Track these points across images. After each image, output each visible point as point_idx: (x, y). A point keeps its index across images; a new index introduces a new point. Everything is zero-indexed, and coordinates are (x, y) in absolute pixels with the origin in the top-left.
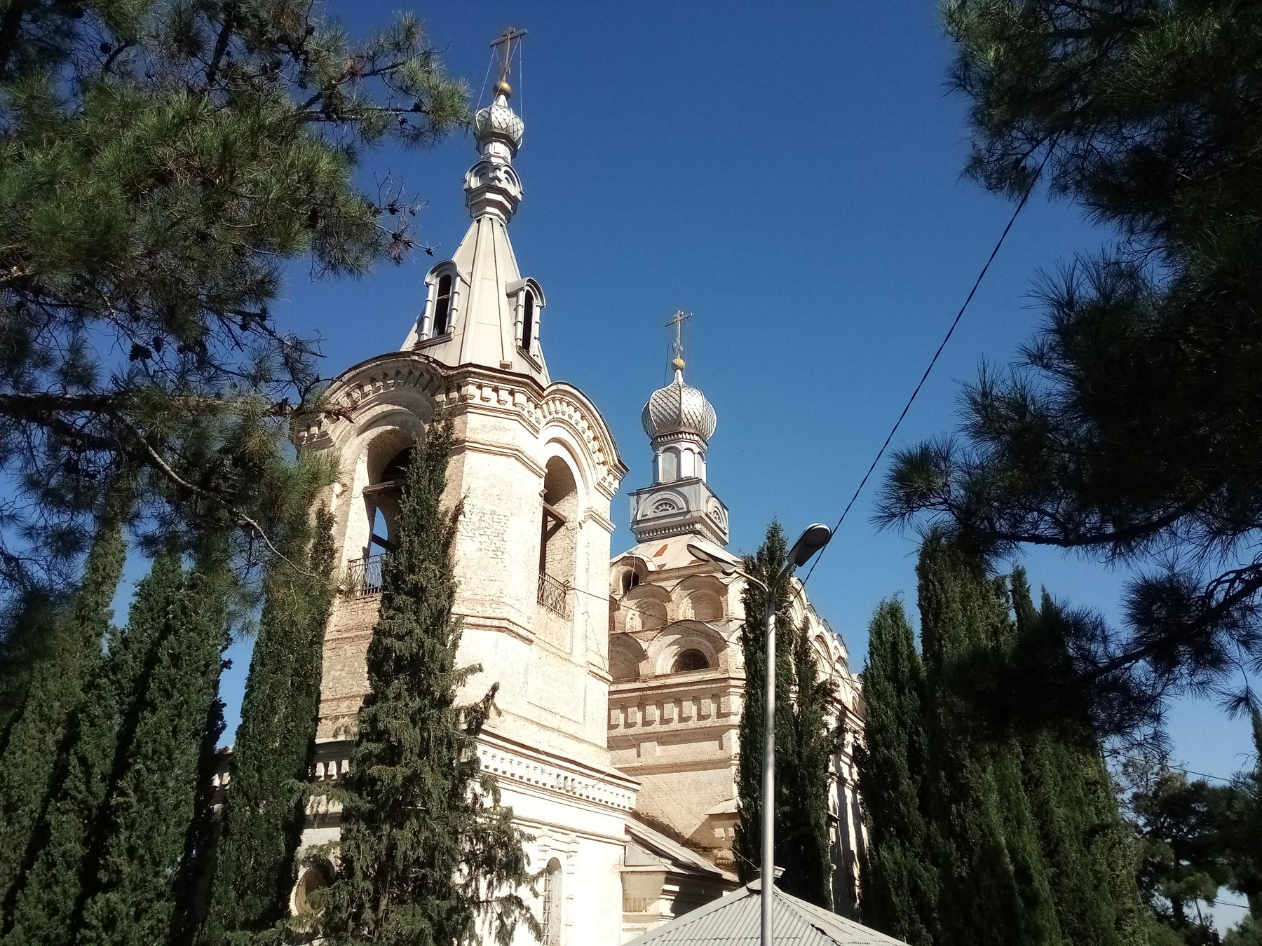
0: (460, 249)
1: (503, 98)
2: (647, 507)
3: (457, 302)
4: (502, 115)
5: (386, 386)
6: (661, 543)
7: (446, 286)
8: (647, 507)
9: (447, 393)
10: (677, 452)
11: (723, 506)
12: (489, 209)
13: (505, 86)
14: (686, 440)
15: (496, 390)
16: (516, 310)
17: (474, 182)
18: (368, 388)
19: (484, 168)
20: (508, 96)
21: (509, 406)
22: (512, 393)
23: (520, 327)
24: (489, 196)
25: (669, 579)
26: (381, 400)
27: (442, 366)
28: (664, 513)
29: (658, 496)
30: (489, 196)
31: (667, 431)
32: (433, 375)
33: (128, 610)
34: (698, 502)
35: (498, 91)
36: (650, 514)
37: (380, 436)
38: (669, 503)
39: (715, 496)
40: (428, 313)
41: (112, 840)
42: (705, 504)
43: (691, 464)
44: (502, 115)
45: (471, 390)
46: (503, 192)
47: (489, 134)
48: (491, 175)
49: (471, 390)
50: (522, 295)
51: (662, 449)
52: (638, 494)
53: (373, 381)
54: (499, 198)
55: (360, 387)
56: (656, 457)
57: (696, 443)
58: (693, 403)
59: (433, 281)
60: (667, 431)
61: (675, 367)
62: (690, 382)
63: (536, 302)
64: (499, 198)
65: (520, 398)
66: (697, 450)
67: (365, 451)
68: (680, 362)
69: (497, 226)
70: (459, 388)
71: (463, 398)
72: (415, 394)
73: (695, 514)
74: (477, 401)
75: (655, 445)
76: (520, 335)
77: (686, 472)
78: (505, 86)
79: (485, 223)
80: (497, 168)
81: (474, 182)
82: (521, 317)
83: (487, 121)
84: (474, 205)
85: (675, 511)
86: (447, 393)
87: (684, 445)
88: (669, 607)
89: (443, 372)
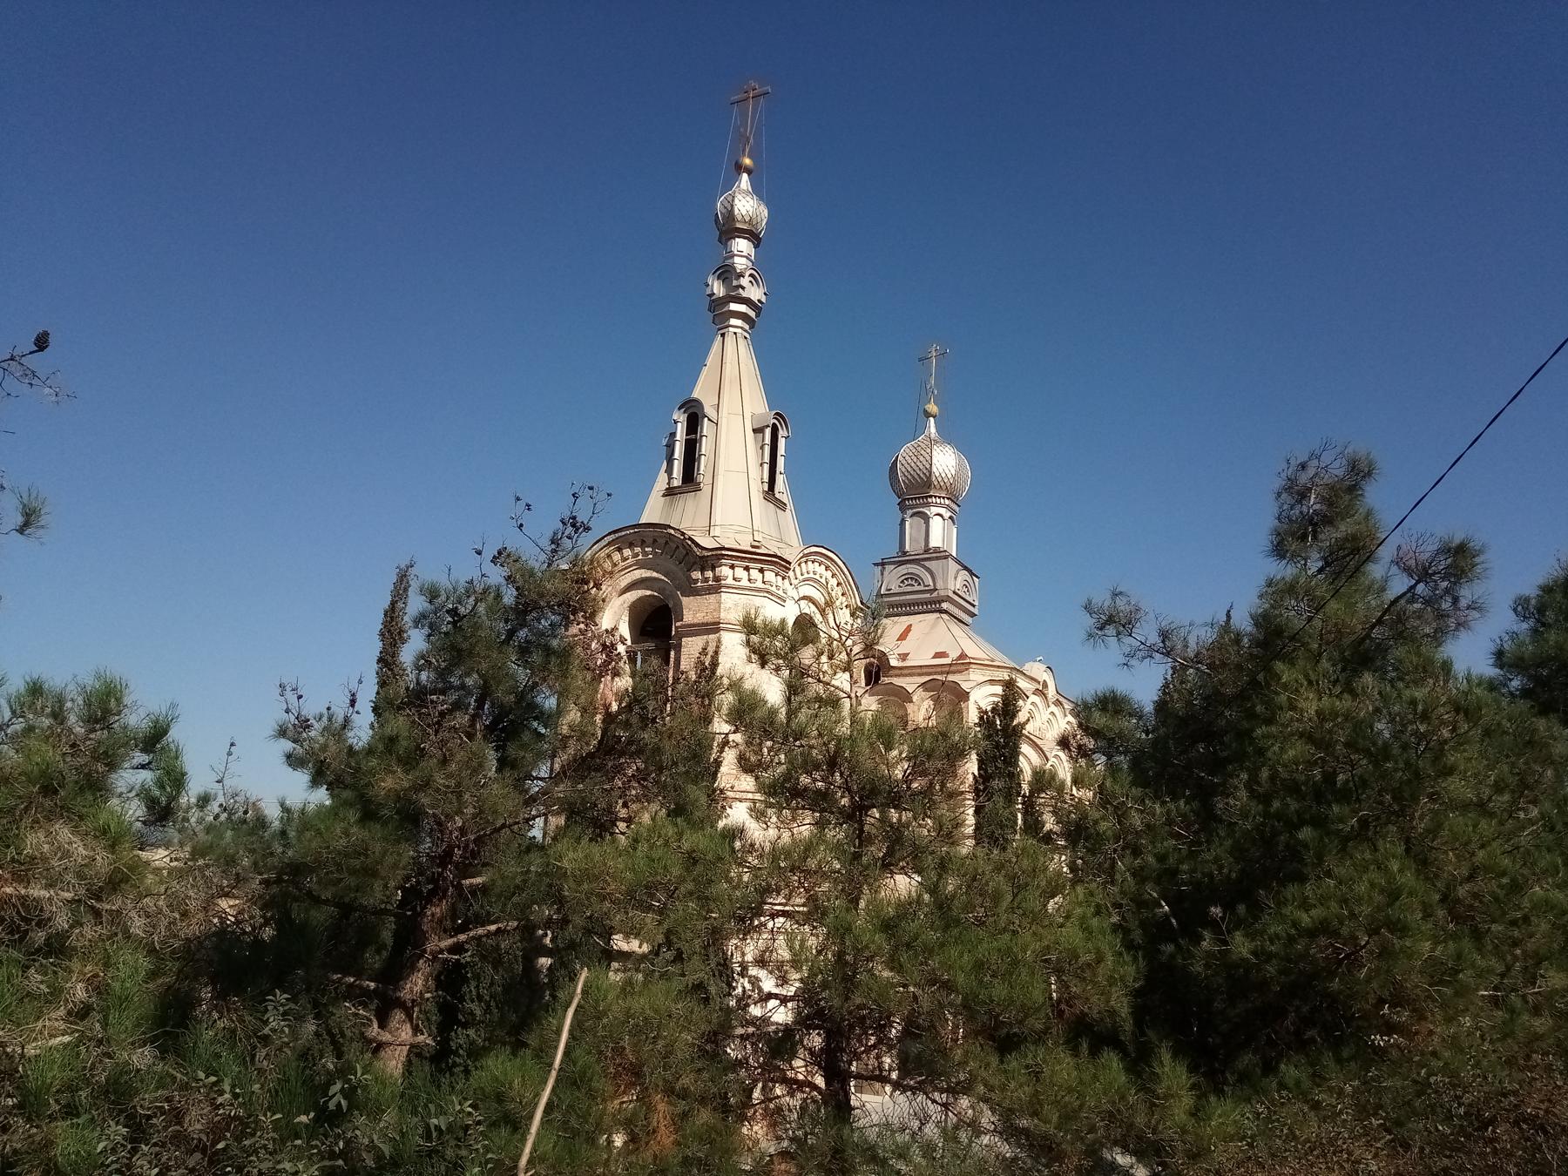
0: (705, 369)
1: (745, 176)
2: (892, 580)
3: (705, 446)
4: (746, 205)
5: (645, 554)
6: (905, 621)
7: (694, 423)
8: (892, 580)
9: (703, 570)
10: (926, 518)
11: (972, 574)
12: (733, 321)
13: (747, 161)
14: (936, 505)
15: (747, 569)
16: (762, 448)
17: (718, 289)
18: (627, 552)
19: (727, 273)
20: (749, 172)
21: (759, 584)
22: (761, 571)
23: (766, 467)
24: (734, 307)
25: (908, 679)
26: (641, 565)
27: (697, 545)
28: (909, 589)
29: (903, 569)
30: (734, 307)
31: (915, 492)
32: (689, 552)
33: (376, 666)
34: (945, 581)
35: (739, 168)
36: (895, 589)
37: (640, 599)
38: (916, 579)
39: (966, 568)
40: (676, 455)
41: (465, 989)
42: (953, 581)
43: (941, 533)
44: (746, 205)
45: (724, 571)
46: (747, 301)
47: (729, 229)
48: (735, 283)
49: (724, 571)
50: (768, 432)
51: (910, 512)
52: (883, 564)
53: (631, 545)
54: (742, 308)
55: (619, 550)
56: (903, 521)
57: (948, 507)
58: (945, 462)
59: (681, 418)
60: (915, 492)
61: (928, 415)
62: (947, 437)
63: (782, 433)
64: (742, 308)
65: (769, 576)
66: (947, 514)
67: (627, 613)
68: (932, 408)
69: (741, 340)
70: (713, 568)
71: (717, 579)
72: (671, 565)
73: (942, 593)
74: (730, 581)
75: (903, 507)
76: (766, 478)
77: (935, 541)
78: (747, 161)
79: (729, 339)
80: (741, 275)
81: (718, 289)
82: (767, 459)
83: (730, 215)
84: (718, 312)
85: (921, 588)
86: (703, 570)
87: (934, 510)
88: (910, 708)
89: (698, 552)
